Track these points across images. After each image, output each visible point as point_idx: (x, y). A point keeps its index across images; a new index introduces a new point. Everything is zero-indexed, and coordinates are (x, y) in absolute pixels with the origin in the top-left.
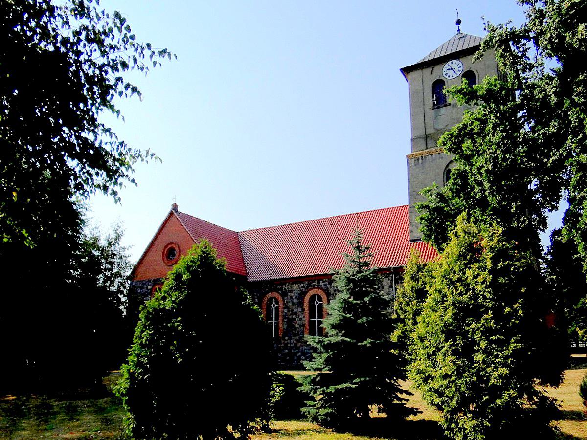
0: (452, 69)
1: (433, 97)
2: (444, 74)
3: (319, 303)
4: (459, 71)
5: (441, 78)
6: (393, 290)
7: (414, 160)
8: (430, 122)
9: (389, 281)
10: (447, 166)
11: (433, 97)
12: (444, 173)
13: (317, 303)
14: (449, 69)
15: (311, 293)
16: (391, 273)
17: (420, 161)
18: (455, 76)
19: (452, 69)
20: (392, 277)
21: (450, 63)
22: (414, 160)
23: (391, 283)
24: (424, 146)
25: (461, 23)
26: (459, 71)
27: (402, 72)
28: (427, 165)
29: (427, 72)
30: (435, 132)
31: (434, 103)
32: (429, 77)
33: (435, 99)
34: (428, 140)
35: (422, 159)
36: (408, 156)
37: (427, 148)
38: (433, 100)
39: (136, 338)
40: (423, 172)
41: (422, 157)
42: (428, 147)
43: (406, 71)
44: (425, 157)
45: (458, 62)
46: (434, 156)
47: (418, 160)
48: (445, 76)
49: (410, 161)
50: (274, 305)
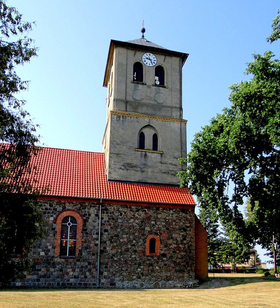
0: (149, 59)
1: (134, 74)
2: (143, 60)
3: (71, 224)
4: (145, 61)
5: (141, 62)
6: (99, 219)
7: (116, 116)
8: (130, 91)
9: (96, 211)
10: (141, 129)
11: (134, 74)
12: (139, 133)
13: (69, 224)
14: (147, 58)
15: (65, 214)
16: (99, 204)
17: (121, 119)
18: (151, 65)
19: (149, 59)
20: (99, 207)
21: (148, 54)
22: (116, 116)
23: (97, 212)
24: (124, 109)
25: (146, 30)
26: (154, 63)
27: (111, 43)
28: (126, 123)
29: (131, 53)
30: (133, 100)
31: (134, 78)
32: (133, 57)
33: (135, 75)
34: (128, 104)
35: (123, 118)
36: (111, 111)
37: (126, 111)
38: (134, 76)
39: (217, 268)
40: (123, 128)
41: (123, 116)
42: (127, 110)
43: (115, 44)
44: (126, 118)
45: (154, 56)
46: (132, 118)
47: (120, 117)
48: (144, 62)
49: (113, 116)
50: (69, 224)
